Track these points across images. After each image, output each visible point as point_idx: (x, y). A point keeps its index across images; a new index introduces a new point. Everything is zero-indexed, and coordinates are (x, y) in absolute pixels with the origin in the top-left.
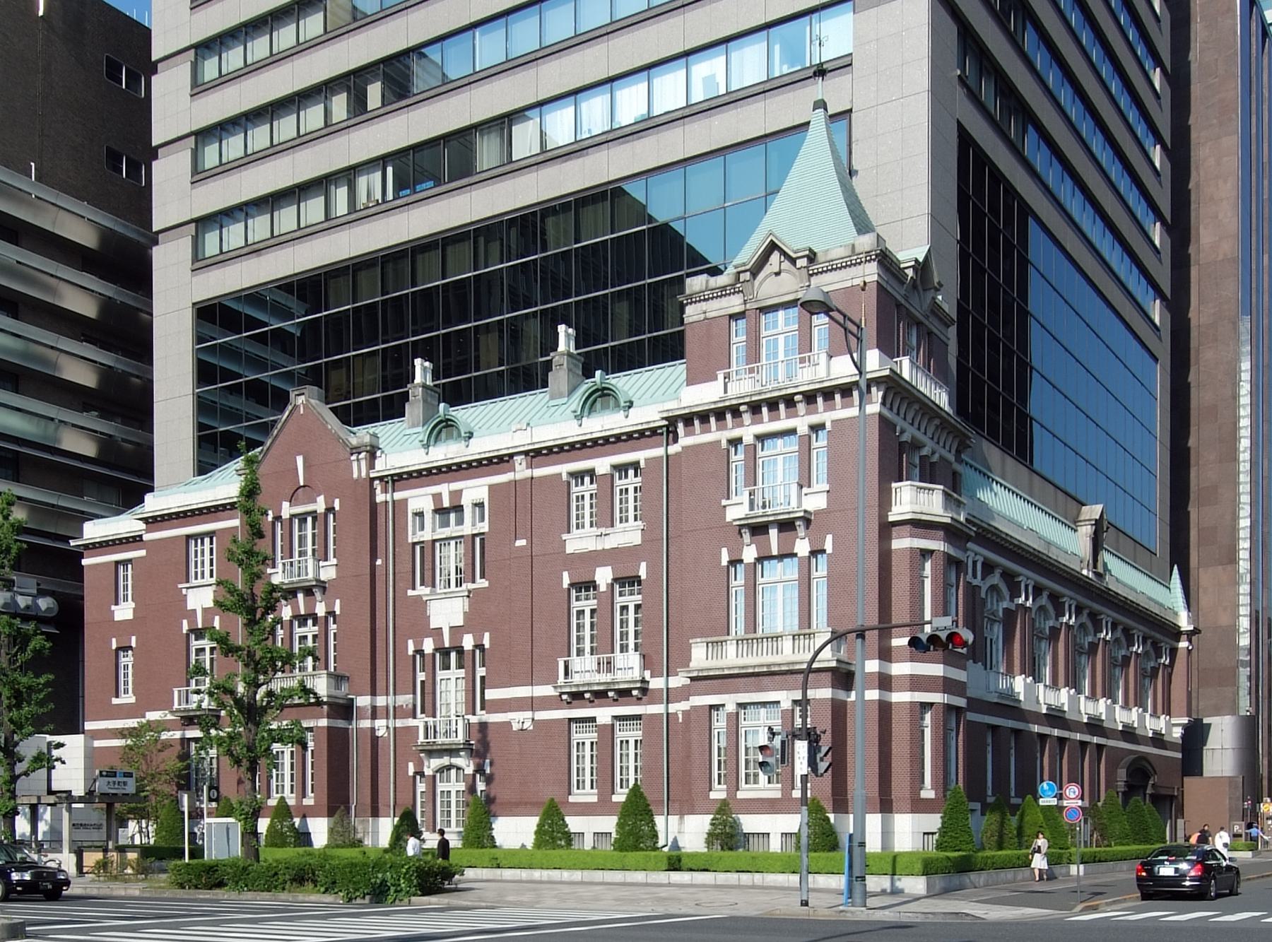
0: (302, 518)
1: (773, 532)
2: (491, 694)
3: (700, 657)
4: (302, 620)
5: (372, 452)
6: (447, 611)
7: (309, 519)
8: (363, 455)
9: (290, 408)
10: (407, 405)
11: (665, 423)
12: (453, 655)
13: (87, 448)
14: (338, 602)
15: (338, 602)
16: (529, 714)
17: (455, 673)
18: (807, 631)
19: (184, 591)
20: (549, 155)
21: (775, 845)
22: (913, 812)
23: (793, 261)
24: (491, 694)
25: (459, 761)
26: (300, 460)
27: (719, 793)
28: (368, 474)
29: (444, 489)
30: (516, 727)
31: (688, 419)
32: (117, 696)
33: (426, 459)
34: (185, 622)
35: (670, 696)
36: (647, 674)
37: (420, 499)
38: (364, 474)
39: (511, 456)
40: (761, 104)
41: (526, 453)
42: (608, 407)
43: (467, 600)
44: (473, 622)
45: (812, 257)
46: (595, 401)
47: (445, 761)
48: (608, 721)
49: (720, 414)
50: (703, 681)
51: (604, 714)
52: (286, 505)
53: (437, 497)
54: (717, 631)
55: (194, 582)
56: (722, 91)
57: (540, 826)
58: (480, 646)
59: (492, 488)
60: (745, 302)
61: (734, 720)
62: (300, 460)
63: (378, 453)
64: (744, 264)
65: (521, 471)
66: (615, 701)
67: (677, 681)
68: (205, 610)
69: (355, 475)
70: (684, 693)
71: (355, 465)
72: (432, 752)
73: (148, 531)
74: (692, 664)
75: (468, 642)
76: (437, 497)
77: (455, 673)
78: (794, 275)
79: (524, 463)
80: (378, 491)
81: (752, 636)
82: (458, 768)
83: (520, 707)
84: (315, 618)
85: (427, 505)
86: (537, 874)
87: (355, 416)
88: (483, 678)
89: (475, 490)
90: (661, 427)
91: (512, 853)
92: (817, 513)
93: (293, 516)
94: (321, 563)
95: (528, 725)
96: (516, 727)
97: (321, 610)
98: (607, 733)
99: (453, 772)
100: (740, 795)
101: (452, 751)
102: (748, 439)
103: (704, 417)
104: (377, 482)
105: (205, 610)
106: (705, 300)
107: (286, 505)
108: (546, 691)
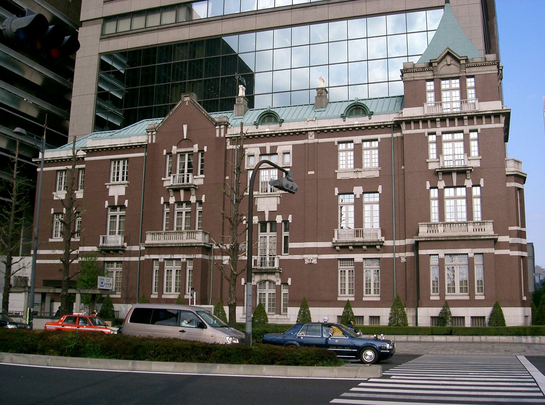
0: (182, 155)
1: (454, 175)
2: (291, 245)
3: (150, 240)
4: (180, 203)
5: (227, 125)
6: (267, 204)
7: (187, 155)
8: (154, 133)
9: (181, 102)
10: (235, 106)
11: (393, 123)
12: (268, 225)
13: (34, 113)
14: (204, 196)
15: (204, 196)
16: (316, 256)
17: (268, 234)
18: (193, 231)
19: (108, 187)
20: (178, 24)
21: (468, 323)
22: (521, 307)
23: (458, 61)
24: (291, 245)
25: (272, 278)
26: (185, 127)
27: (347, 296)
28: (224, 135)
29: (268, 146)
30: (307, 262)
31: (408, 122)
32: (52, 238)
33: (256, 131)
34: (107, 202)
35: (134, 254)
36: (125, 244)
37: (253, 149)
38: (222, 135)
39: (307, 132)
40: (220, 24)
41: (315, 131)
42: (271, 121)
43: (279, 198)
44: (281, 209)
45: (467, 60)
46: (265, 118)
47: (265, 277)
48: (361, 260)
49: (425, 121)
50: (151, 249)
51: (358, 257)
52: (174, 148)
53: (263, 149)
54: (156, 227)
55: (112, 182)
56: (256, 9)
57: (300, 312)
58: (286, 222)
59: (293, 146)
60: (434, 75)
61: (441, 261)
62: (185, 127)
63: (230, 126)
64: (435, 59)
65: (312, 139)
66: (365, 252)
67: (136, 248)
68: (120, 197)
69: (218, 135)
70: (141, 253)
71: (218, 131)
72: (261, 272)
73: (87, 156)
74: (419, 235)
75: (279, 219)
76: (263, 149)
77: (268, 234)
78: (457, 66)
79: (314, 136)
80: (228, 143)
81: (193, 231)
82: (270, 282)
83: (311, 251)
84: (188, 203)
85: (257, 152)
86: (490, 338)
87: (211, 107)
88: (286, 238)
89: (285, 146)
90: (390, 125)
91: (513, 328)
92: (475, 168)
93: (178, 153)
94: (195, 177)
95: (315, 261)
96: (307, 262)
97: (193, 199)
98: (359, 267)
99: (267, 283)
100: (163, 297)
101: (271, 272)
102: (439, 132)
103: (488, 116)
104: (228, 139)
105: (120, 197)
106: (414, 72)
107: (174, 148)
108: (95, 249)
